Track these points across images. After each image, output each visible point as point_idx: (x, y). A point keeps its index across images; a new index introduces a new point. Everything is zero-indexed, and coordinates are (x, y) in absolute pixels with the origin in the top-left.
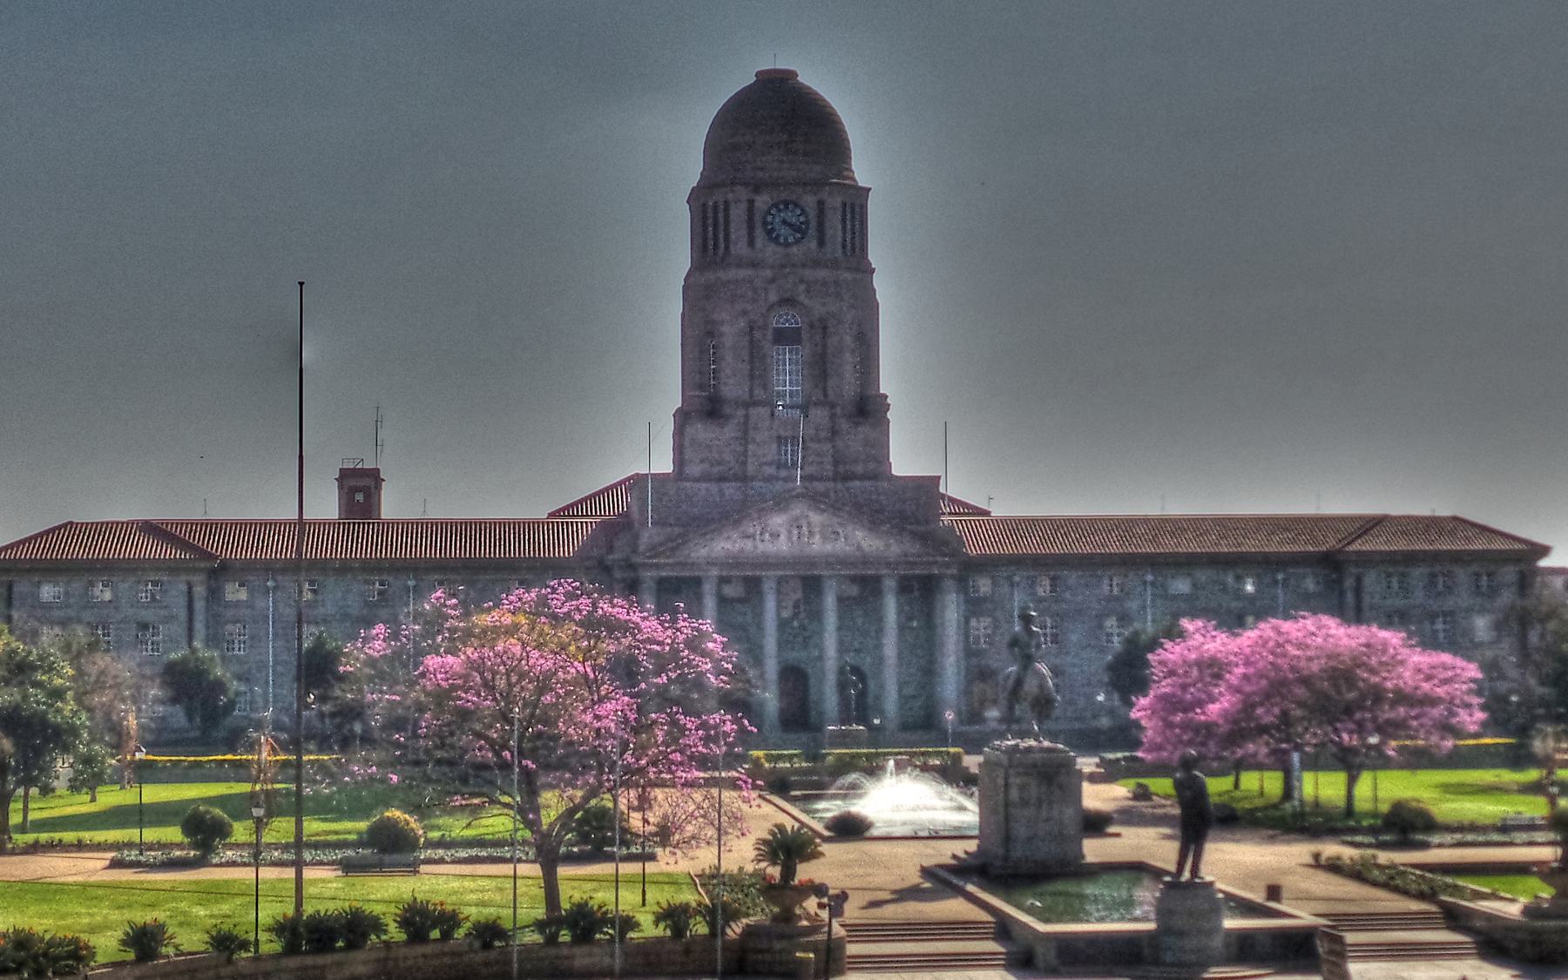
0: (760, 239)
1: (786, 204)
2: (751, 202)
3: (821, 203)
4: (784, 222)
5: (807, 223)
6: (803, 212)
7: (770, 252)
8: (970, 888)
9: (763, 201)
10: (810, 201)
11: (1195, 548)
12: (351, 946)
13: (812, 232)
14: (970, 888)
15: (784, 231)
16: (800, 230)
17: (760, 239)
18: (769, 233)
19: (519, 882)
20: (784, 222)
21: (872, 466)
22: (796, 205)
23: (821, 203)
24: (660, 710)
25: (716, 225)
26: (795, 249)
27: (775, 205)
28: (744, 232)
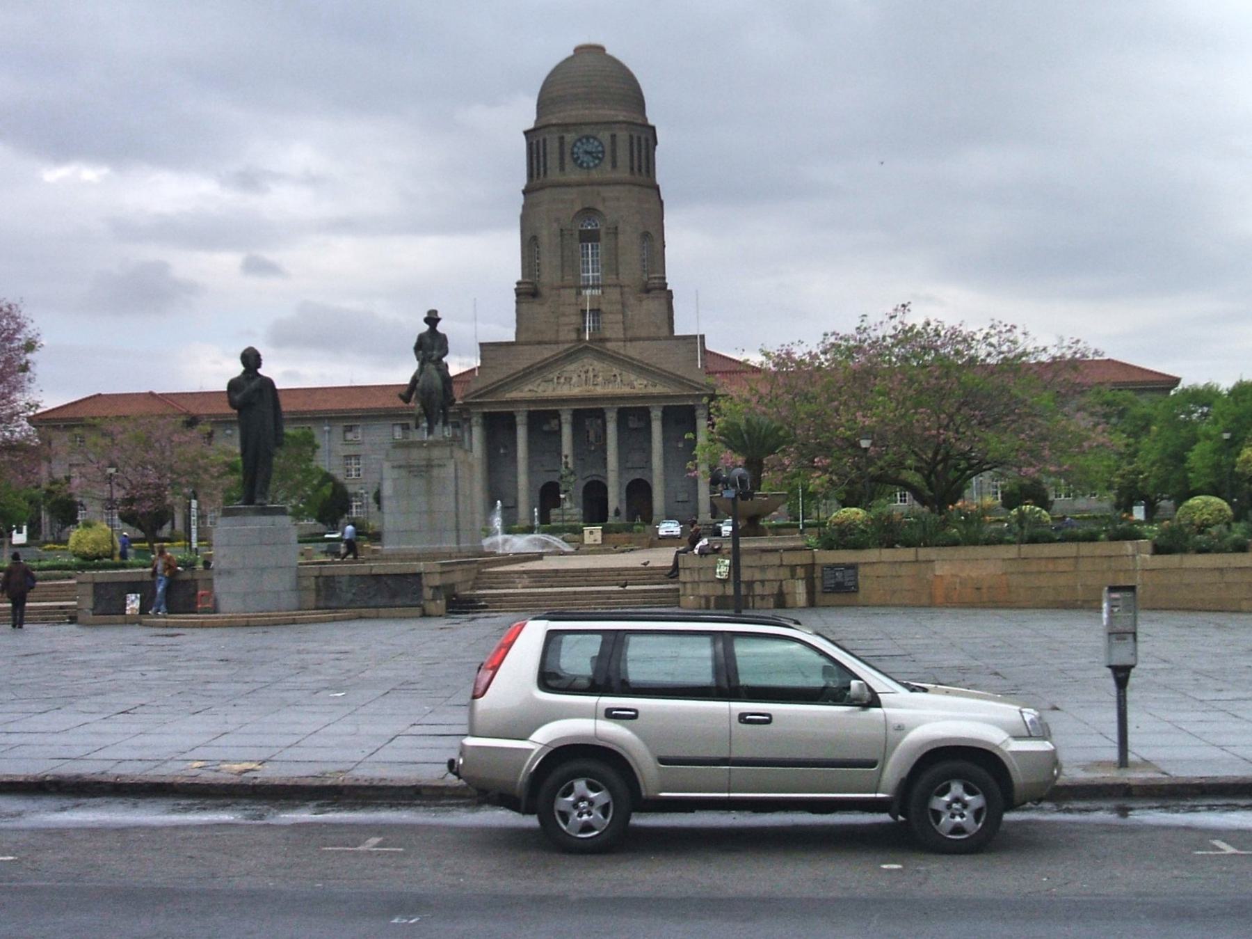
0: (569, 164)
1: (588, 138)
2: (562, 138)
3: (613, 137)
4: (587, 152)
5: (603, 152)
6: (601, 143)
7: (574, 175)
8: (885, 818)
9: (570, 137)
10: (605, 136)
11: (379, 404)
12: (707, 598)
13: (608, 157)
14: (885, 818)
15: (586, 158)
16: (598, 157)
17: (569, 164)
18: (575, 160)
19: (745, 561)
20: (587, 152)
21: (417, 456)
22: (595, 138)
23: (613, 137)
24: (175, 494)
25: (538, 162)
26: (594, 172)
27: (580, 140)
28: (557, 163)
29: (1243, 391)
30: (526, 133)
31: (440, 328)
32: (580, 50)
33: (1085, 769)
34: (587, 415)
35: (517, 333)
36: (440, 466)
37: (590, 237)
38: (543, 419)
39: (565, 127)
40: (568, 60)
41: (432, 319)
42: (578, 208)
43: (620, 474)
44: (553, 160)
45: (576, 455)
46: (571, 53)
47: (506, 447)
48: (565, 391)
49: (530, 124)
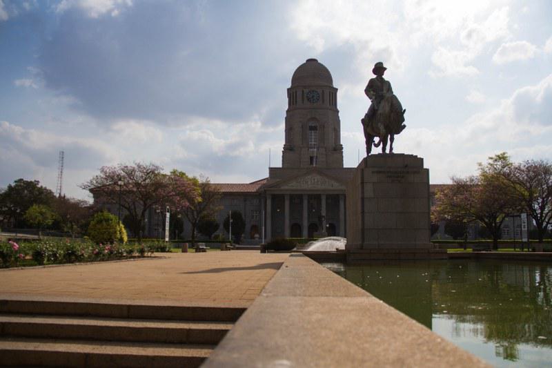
2: (303, 91)
29: (537, 172)
30: (288, 89)
31: (386, 76)
32: (308, 61)
33: (165, 258)
34: (315, 198)
35: (283, 164)
36: (415, 172)
37: (313, 128)
38: (296, 199)
39: (305, 87)
40: (304, 64)
41: (379, 69)
42: (309, 117)
43: (290, 221)
44: (299, 100)
45: (170, 238)
46: (305, 62)
47: (279, 208)
48: (305, 187)
49: (289, 87)
